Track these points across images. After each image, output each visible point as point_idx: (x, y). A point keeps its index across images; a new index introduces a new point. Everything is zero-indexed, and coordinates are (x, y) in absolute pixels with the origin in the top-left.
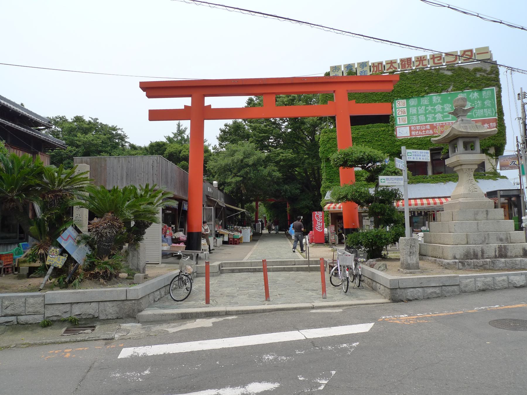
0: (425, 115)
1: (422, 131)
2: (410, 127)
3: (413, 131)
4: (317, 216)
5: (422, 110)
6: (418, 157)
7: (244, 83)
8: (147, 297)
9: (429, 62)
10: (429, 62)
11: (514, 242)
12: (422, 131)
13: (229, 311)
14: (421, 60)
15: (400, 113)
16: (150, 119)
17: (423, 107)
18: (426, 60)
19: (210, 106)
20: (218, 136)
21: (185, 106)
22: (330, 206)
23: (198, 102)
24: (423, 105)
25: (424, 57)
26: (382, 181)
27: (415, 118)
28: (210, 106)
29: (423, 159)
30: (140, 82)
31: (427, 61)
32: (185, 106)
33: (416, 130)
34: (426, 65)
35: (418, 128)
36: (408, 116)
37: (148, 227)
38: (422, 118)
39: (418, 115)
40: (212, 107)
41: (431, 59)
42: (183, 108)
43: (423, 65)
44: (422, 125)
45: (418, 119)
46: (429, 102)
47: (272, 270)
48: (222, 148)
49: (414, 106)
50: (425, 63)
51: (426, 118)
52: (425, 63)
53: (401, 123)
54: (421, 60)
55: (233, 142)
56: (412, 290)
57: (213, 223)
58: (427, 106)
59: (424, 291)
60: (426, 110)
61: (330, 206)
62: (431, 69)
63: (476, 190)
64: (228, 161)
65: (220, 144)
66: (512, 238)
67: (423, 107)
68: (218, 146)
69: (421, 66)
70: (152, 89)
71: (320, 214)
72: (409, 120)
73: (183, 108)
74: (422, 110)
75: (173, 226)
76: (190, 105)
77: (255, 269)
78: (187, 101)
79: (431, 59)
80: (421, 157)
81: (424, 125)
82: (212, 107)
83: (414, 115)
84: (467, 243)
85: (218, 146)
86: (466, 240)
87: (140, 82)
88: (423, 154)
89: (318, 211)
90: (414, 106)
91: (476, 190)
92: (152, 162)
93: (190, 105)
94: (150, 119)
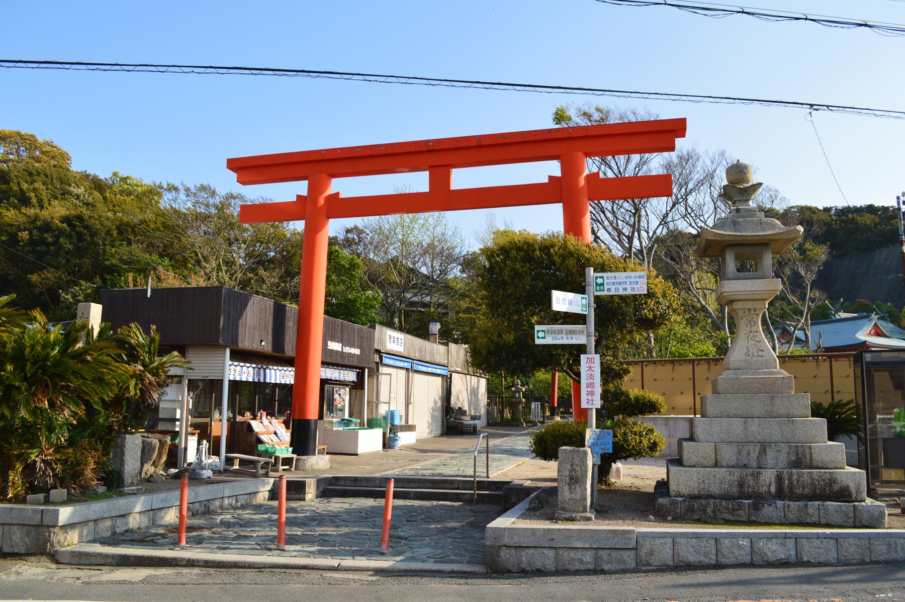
6: (621, 287)
7: (294, 160)
8: (91, 524)
11: (820, 465)
13: (193, 561)
21: (550, 177)
23: (570, 169)
29: (633, 289)
30: (685, 119)
32: (550, 177)
42: (547, 181)
47: (412, 496)
56: (531, 551)
59: (557, 555)
63: (760, 353)
66: (815, 456)
73: (547, 181)
76: (560, 175)
77: (409, 493)
78: (301, 188)
80: (629, 287)
82: (342, 196)
84: (716, 465)
86: (713, 456)
87: (685, 119)
88: (633, 280)
91: (760, 353)
93: (560, 175)
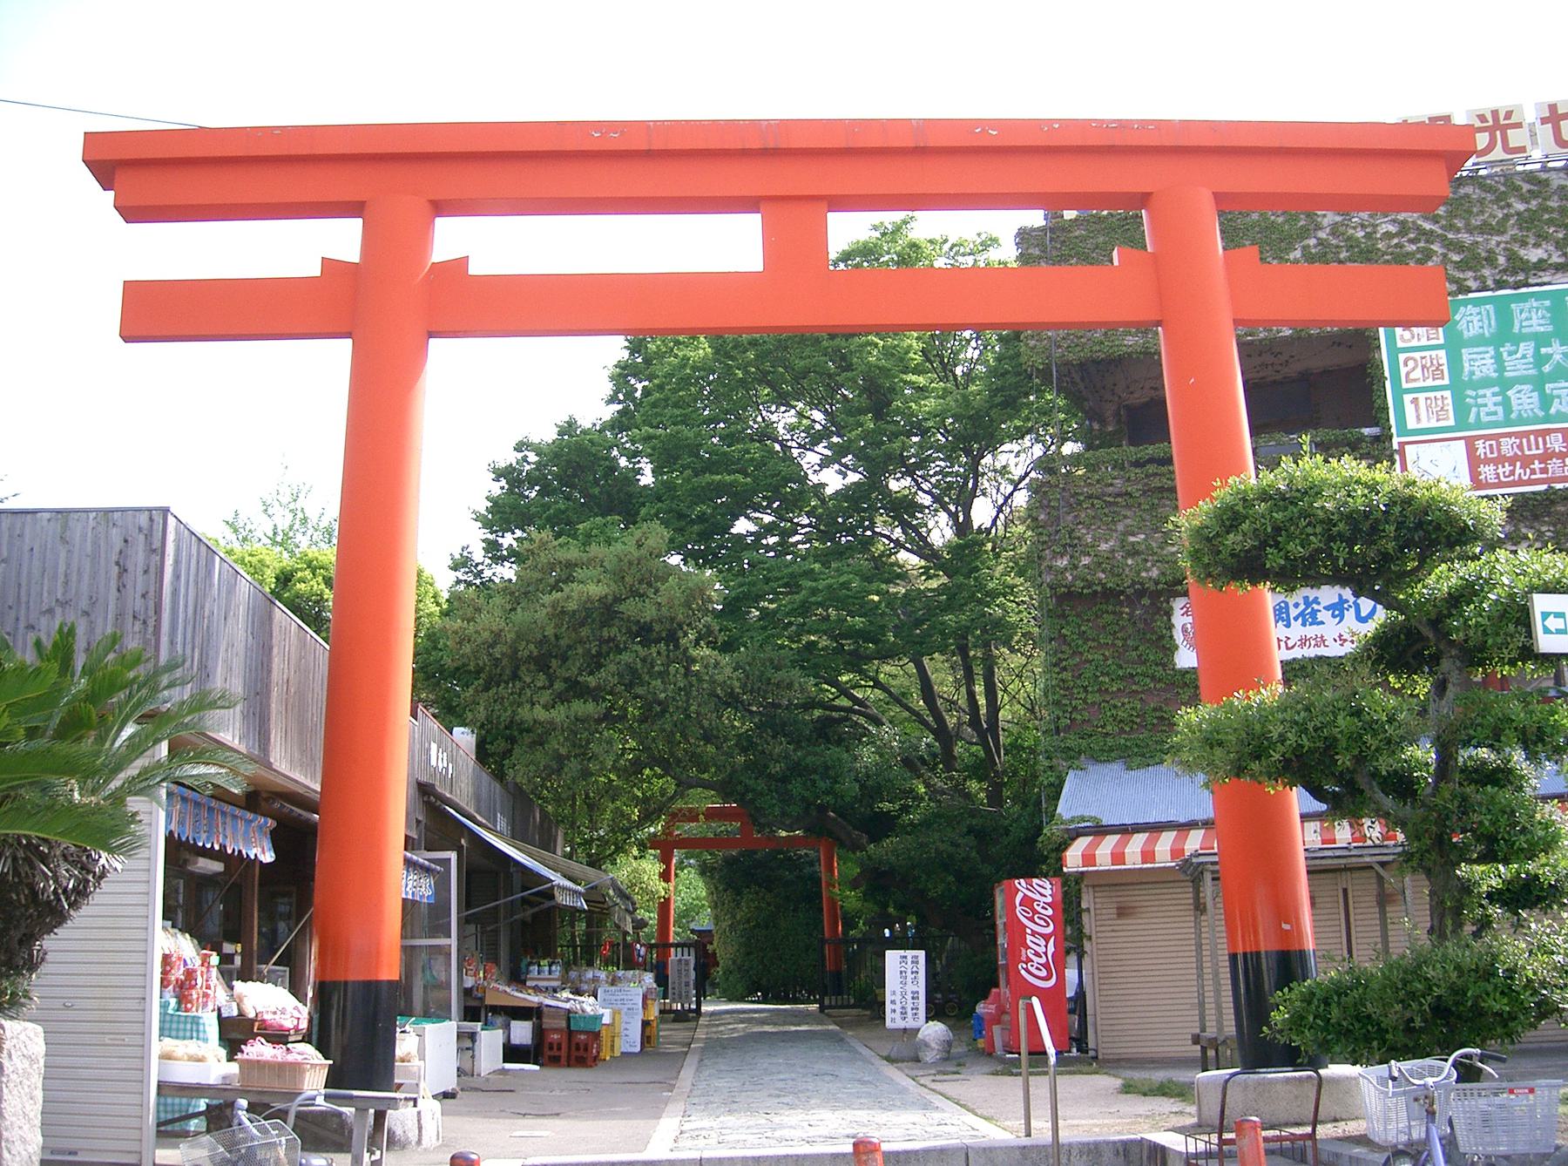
0: (1539, 382)
1: (1526, 462)
2: (1470, 443)
3: (1487, 461)
4: (1028, 902)
5: (1519, 361)
7: (657, 145)
9: (1533, 135)
10: (1533, 135)
12: (1526, 462)
14: (1496, 125)
15: (1417, 374)
16: (130, 334)
17: (1526, 348)
18: (1519, 125)
19: (463, 262)
20: (482, 506)
22: (1093, 846)
24: (1523, 338)
25: (1509, 115)
26: (1553, 623)
27: (1489, 397)
28: (463, 262)
31: (1525, 131)
33: (1500, 460)
34: (1522, 149)
35: (1508, 446)
36: (1458, 387)
37: (60, 918)
38: (1524, 399)
39: (1504, 384)
40: (473, 270)
41: (1544, 121)
43: (1506, 149)
44: (1526, 434)
45: (1506, 404)
46: (1553, 321)
48: (498, 559)
49: (1479, 341)
50: (1515, 138)
51: (1546, 401)
52: (1515, 138)
53: (1424, 424)
54: (1496, 125)
55: (563, 524)
57: (453, 941)
58: (1541, 340)
60: (1540, 360)
61: (1093, 846)
62: (1544, 169)
64: (537, 614)
65: (492, 547)
67: (1526, 348)
68: (478, 555)
69: (1498, 154)
70: (146, 172)
71: (1043, 891)
72: (1461, 410)
74: (1519, 361)
75: (228, 948)
78: (341, 239)
79: (1544, 121)
81: (1537, 433)
82: (473, 270)
83: (1486, 383)
85: (478, 555)
89: (1029, 874)
90: (1479, 341)
92: (118, 544)
94: (130, 334)
